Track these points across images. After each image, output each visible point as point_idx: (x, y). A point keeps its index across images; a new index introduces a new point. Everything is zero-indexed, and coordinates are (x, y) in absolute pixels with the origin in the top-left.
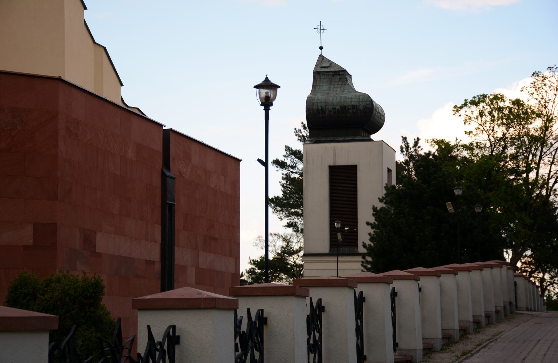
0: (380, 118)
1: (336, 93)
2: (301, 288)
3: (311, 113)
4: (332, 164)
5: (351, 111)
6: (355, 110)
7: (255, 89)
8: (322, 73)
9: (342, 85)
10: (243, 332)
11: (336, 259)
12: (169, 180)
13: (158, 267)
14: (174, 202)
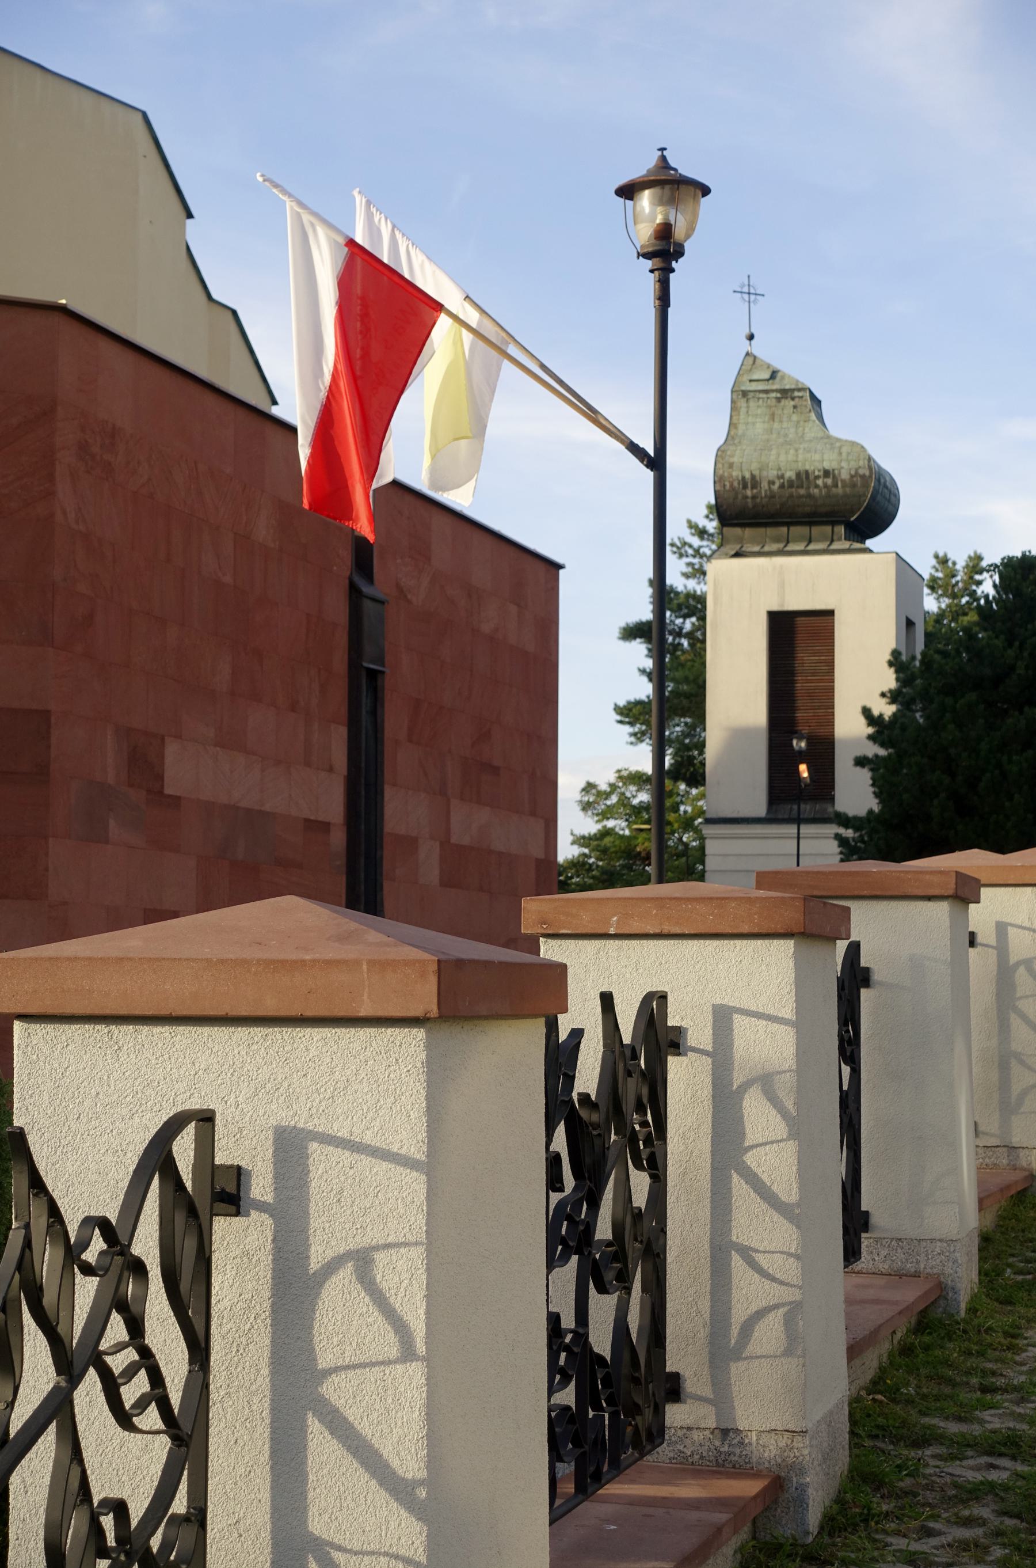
0: (889, 501)
1: (786, 441)
2: (825, 903)
3: (724, 486)
4: (775, 607)
5: (820, 482)
6: (829, 481)
7: (622, 200)
8: (751, 395)
9: (798, 422)
10: (585, 1098)
11: (796, 831)
12: (367, 604)
13: (338, 839)
14: (384, 666)
